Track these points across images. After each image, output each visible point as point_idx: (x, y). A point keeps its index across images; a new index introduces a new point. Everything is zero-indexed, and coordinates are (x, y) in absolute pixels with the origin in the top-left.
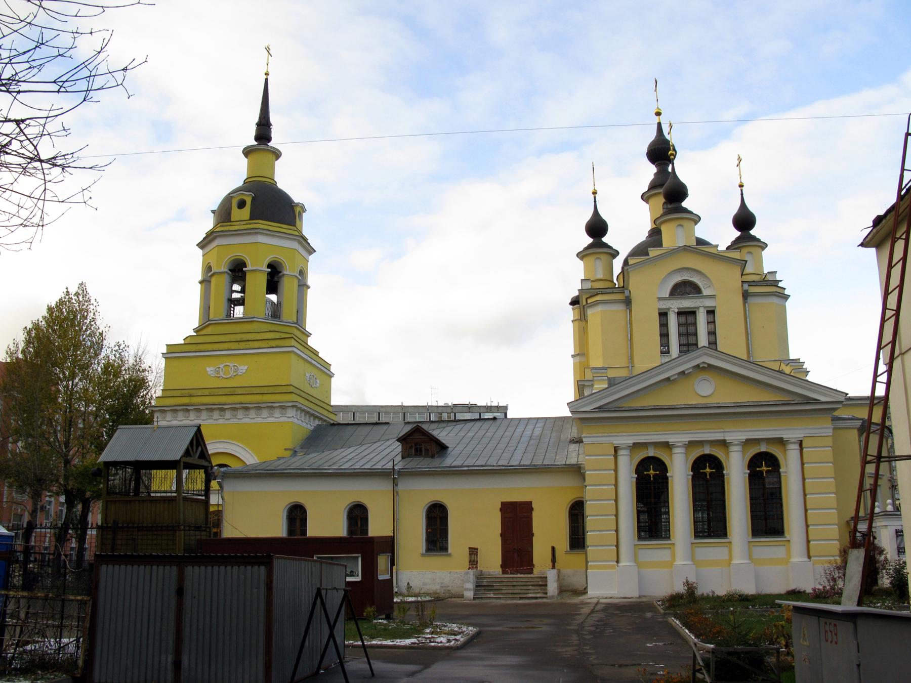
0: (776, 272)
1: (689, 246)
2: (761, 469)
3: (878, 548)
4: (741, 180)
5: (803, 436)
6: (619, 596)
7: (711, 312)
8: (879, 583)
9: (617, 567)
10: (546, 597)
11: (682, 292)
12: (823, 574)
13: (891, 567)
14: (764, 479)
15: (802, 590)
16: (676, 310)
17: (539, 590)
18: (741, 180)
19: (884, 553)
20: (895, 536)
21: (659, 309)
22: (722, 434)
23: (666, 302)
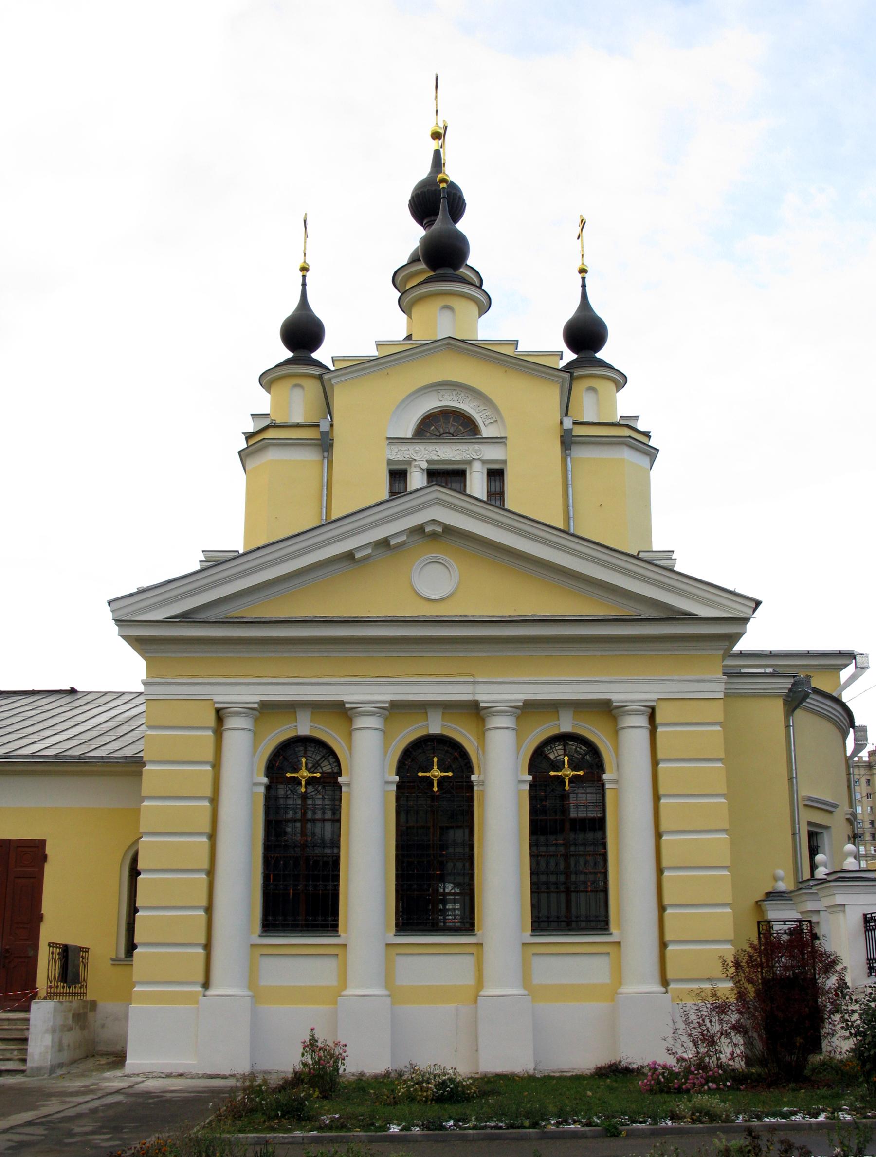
0: (638, 416)
1: (463, 341)
2: (559, 773)
3: (821, 954)
4: (583, 260)
5: (656, 696)
6: (201, 1072)
7: (496, 475)
8: (824, 1050)
9: (201, 998)
10: (23, 1071)
11: (439, 432)
12: (681, 1026)
13: (856, 1007)
14: (565, 797)
15: (634, 1066)
16: (425, 465)
17: (15, 1053)
18: (583, 260)
19: (838, 968)
20: (863, 930)
21: (389, 462)
22: (469, 688)
23: (404, 448)
